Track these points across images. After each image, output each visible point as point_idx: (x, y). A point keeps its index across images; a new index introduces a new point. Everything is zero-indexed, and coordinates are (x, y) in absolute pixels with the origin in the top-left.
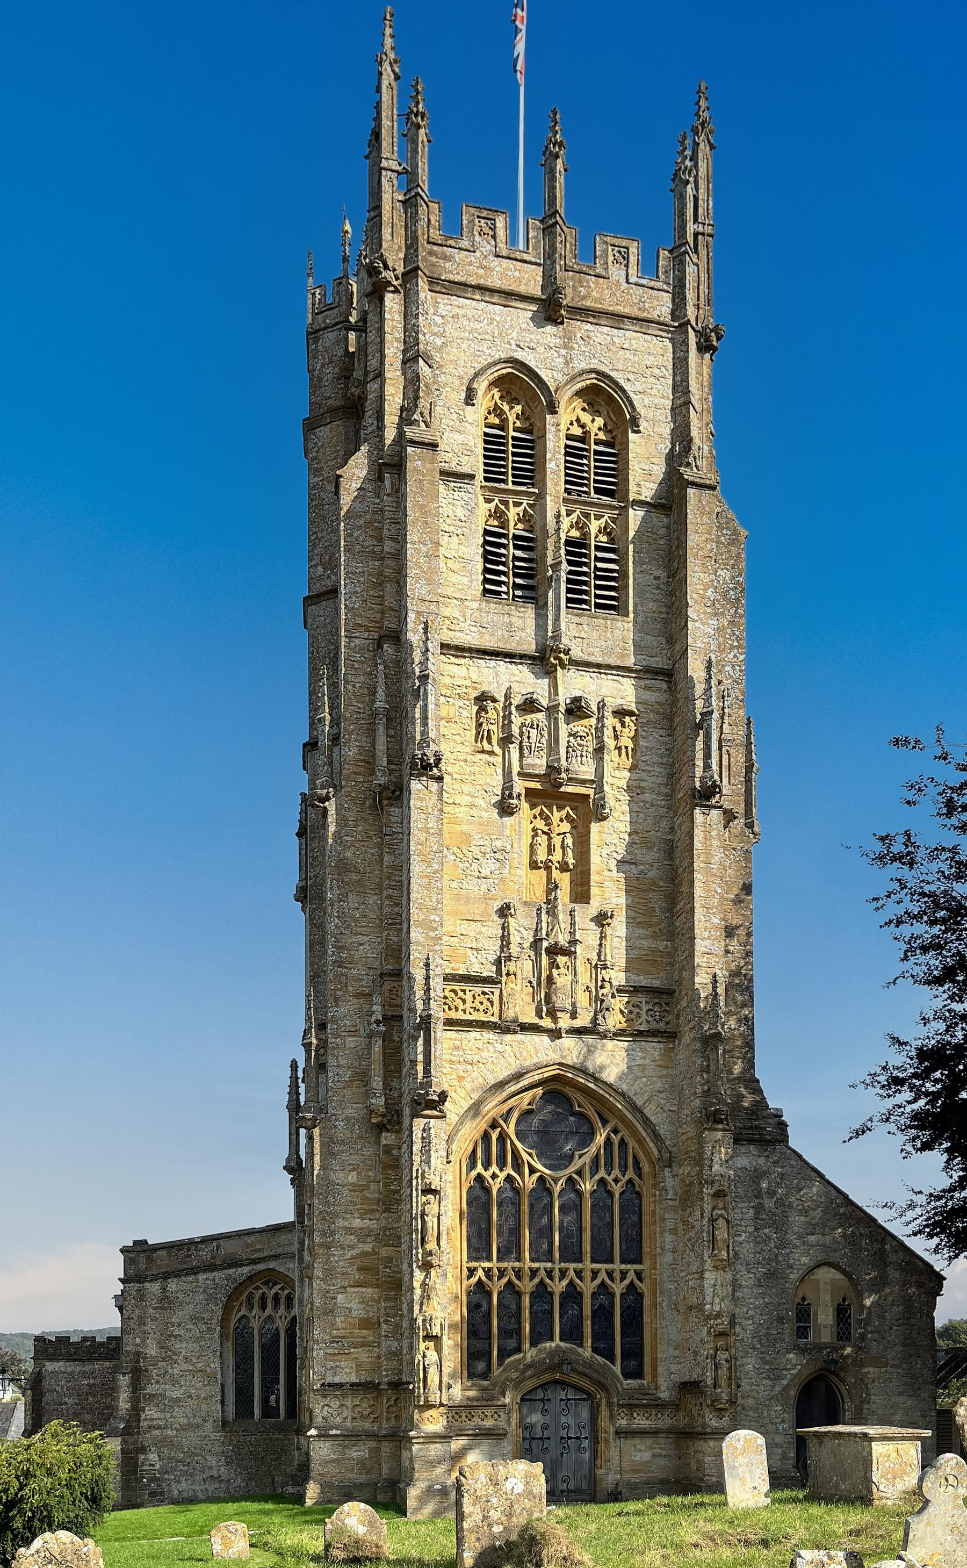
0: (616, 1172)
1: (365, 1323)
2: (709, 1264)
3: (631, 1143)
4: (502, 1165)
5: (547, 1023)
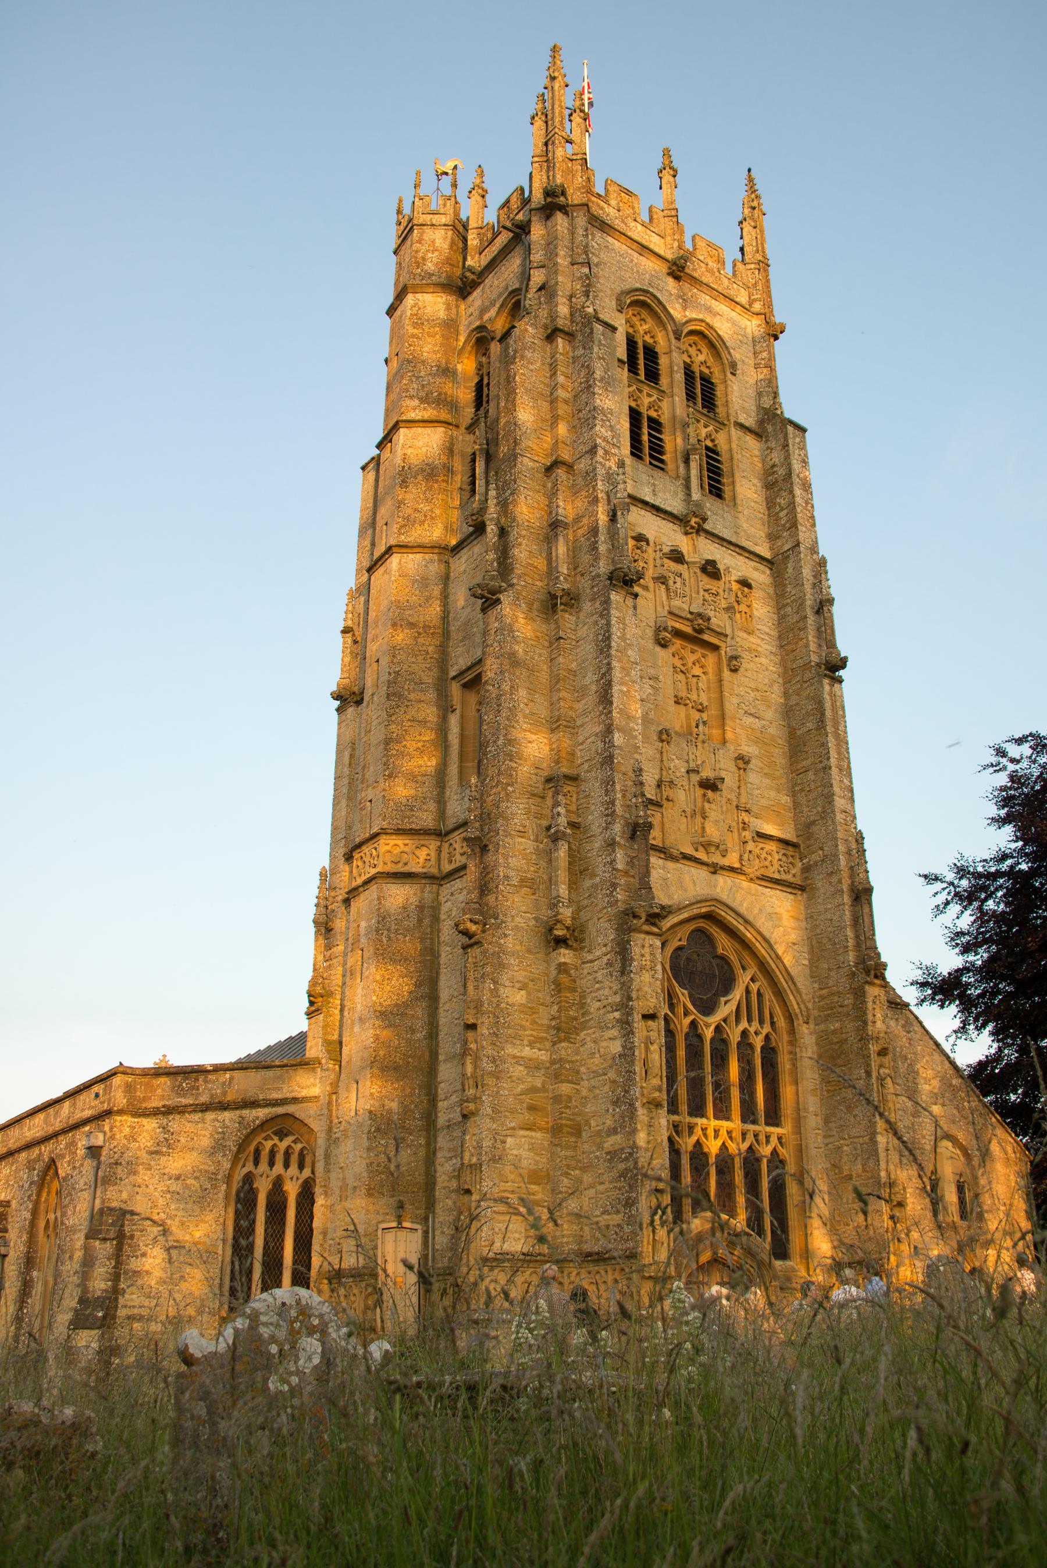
5: (701, 855)
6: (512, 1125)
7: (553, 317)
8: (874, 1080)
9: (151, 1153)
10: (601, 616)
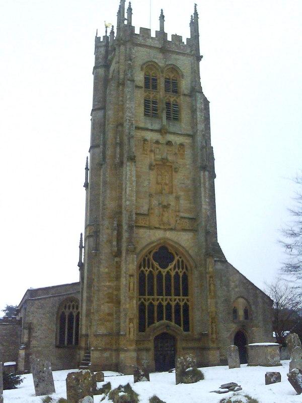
0: (181, 269)
1: (110, 314)
5: (162, 227)
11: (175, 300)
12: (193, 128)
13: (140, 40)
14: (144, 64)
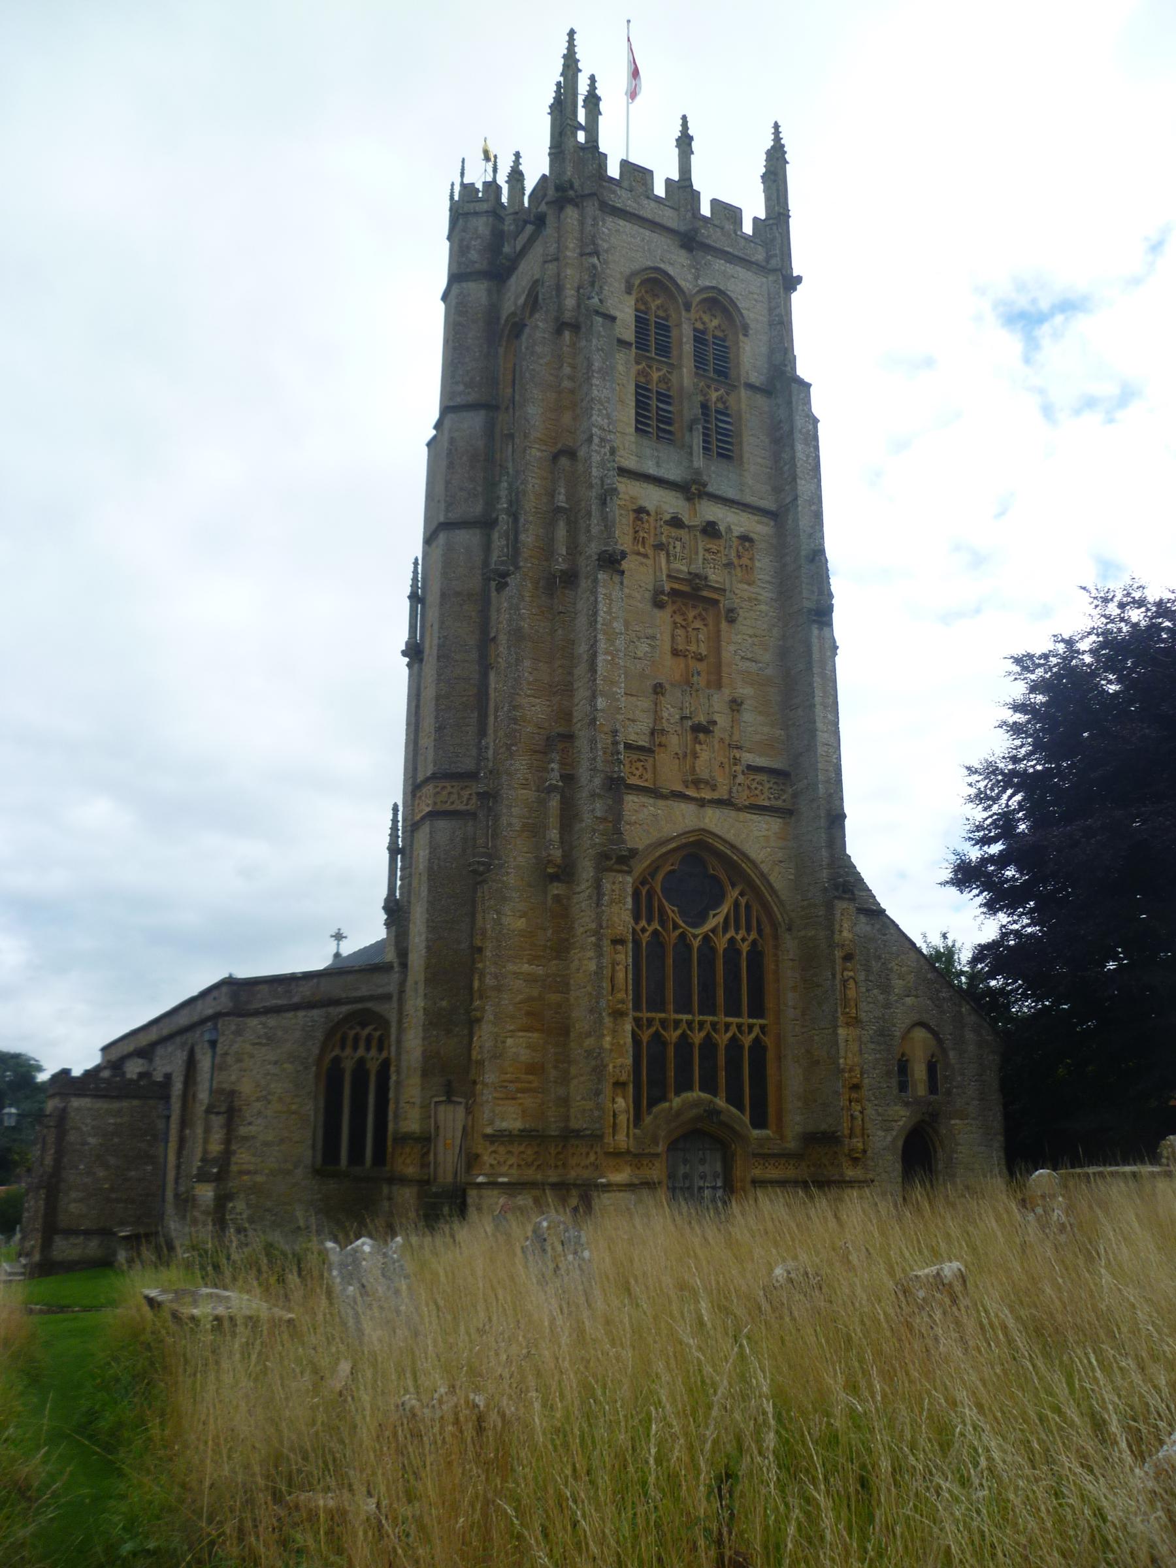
1: (533, 1069)
2: (841, 1019)
3: (755, 907)
4: (649, 921)
5: (691, 792)
6: (512, 1028)
7: (560, 309)
8: (837, 981)
9: (254, 1044)
10: (592, 592)
11: (727, 1027)
12: (777, 490)
13: (622, 199)
14: (634, 274)
